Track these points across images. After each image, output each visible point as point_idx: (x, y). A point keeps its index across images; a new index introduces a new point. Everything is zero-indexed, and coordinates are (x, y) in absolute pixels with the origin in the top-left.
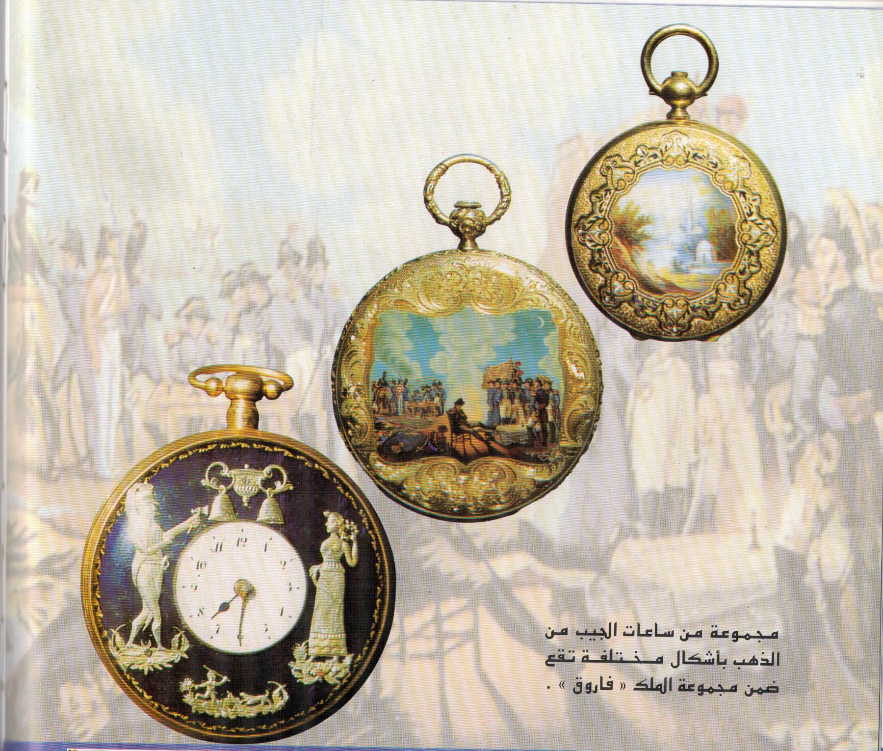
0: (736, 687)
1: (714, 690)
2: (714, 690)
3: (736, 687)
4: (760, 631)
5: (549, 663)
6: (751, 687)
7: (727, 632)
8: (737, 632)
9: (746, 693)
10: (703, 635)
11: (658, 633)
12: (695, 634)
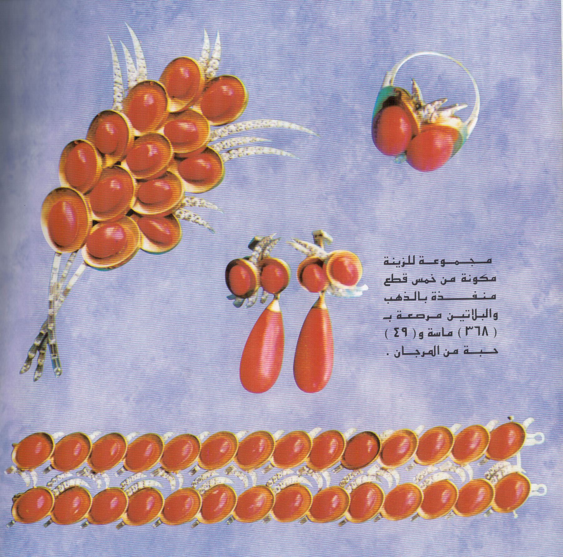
0: (454, 278)
1: (429, 281)
2: (429, 281)
3: (454, 278)
4: (496, 348)
5: (387, 284)
6: (445, 279)
7: (438, 260)
8: (444, 260)
9: (413, 283)
10: (408, 281)
11: (420, 298)
12: (395, 298)
